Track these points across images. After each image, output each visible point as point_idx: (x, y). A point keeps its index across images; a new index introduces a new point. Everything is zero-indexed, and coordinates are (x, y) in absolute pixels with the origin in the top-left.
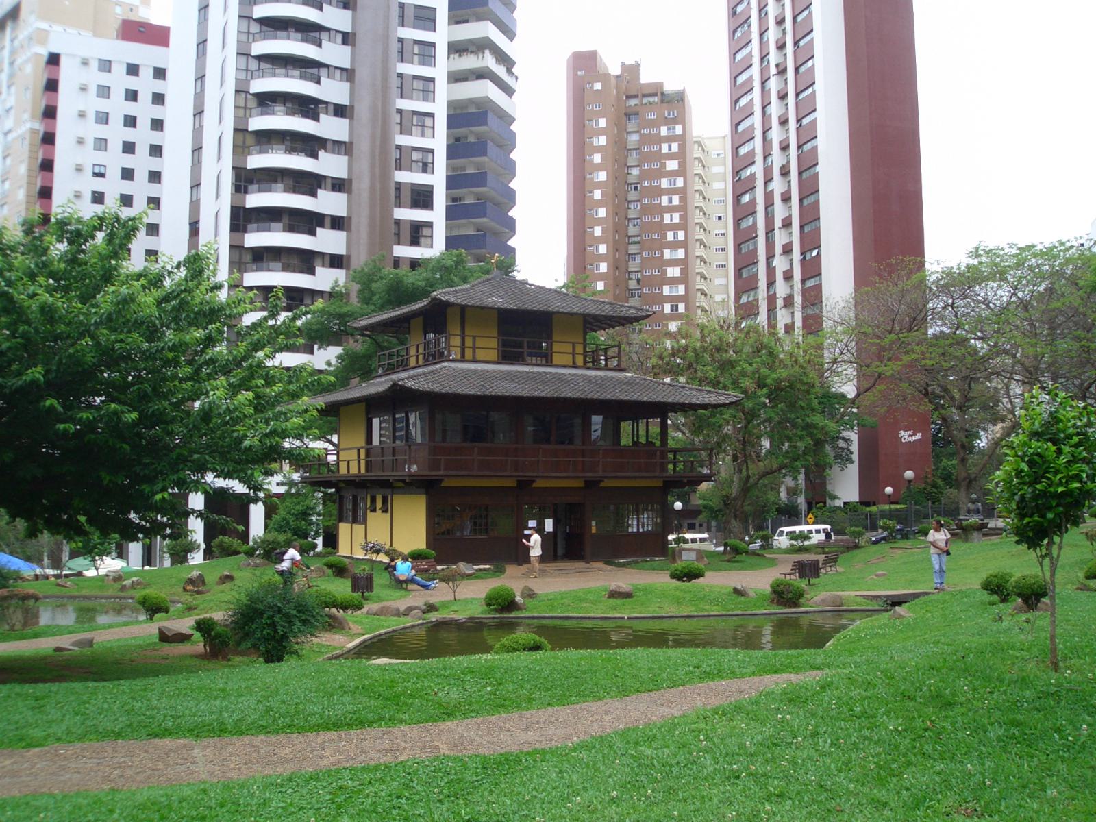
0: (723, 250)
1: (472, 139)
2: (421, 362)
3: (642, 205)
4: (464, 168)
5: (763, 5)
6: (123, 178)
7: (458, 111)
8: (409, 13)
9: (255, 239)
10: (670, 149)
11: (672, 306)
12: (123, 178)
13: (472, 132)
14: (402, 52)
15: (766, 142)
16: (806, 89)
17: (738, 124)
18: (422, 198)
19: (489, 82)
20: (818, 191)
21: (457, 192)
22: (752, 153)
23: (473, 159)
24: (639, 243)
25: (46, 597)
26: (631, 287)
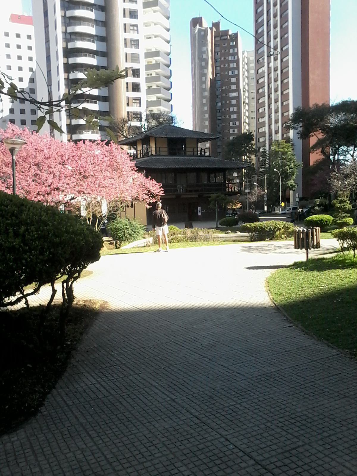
1: (154, 62)
4: (151, 74)
6: (19, 70)
7: (148, 51)
8: (129, 58)
9: (71, 61)
10: (233, 65)
11: (233, 123)
12: (19, 70)
14: (125, 29)
15: (269, 79)
16: (285, 68)
17: (258, 50)
22: (263, 72)
26: (217, 94)
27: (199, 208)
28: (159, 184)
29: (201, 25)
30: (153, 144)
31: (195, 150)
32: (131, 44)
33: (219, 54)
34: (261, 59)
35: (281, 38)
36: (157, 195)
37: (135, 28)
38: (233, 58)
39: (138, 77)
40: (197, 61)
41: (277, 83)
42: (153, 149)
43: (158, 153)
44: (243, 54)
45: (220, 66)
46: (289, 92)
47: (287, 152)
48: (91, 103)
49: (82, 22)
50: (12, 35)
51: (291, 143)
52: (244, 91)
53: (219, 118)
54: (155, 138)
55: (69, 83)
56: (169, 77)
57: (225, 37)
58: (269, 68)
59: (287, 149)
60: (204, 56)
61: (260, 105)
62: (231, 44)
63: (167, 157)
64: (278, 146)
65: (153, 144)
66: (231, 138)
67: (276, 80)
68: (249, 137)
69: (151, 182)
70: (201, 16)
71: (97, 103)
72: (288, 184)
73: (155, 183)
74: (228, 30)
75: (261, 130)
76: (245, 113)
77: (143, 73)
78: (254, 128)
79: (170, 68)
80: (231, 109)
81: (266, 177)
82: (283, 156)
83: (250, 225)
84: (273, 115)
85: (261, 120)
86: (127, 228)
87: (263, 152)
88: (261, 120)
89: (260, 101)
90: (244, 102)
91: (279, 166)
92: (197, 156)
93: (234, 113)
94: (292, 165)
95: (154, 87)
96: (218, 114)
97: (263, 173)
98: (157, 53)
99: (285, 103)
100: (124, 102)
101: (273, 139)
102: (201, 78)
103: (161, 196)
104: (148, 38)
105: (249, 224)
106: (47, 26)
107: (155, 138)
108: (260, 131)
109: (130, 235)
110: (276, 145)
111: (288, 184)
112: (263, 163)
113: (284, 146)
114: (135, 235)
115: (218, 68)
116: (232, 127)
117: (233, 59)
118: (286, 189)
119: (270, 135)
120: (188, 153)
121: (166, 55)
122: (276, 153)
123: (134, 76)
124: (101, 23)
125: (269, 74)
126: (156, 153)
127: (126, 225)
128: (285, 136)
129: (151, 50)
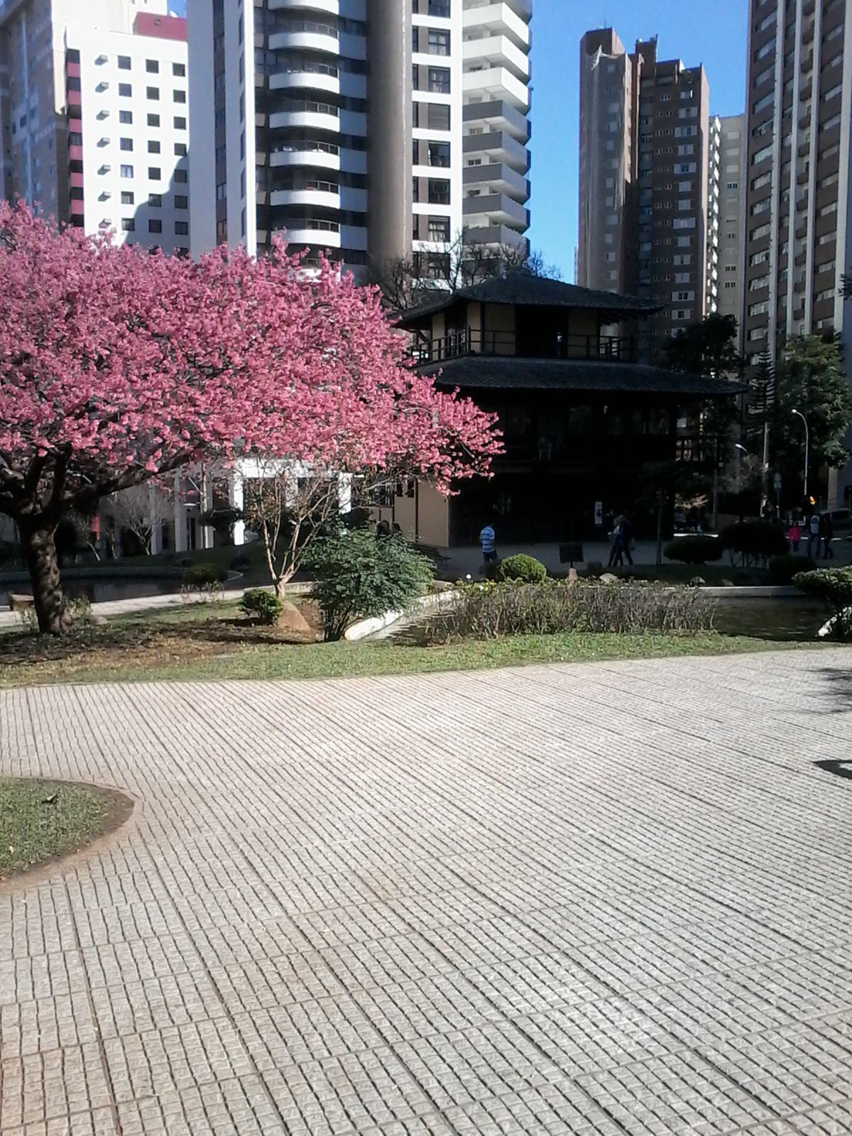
0: (735, 186)
1: (486, 130)
2: (442, 357)
3: (654, 211)
4: (479, 162)
5: (784, 160)
13: (488, 123)
17: (757, 103)
18: (439, 154)
19: (504, 70)
20: (838, 172)
21: (473, 186)
22: (769, 160)
23: (487, 151)
24: (650, 285)
25: (65, 44)
26: (641, 223)
27: (598, 505)
28: (487, 416)
29: (608, 49)
30: (474, 323)
31: (593, 342)
32: (431, 81)
33: (651, 121)
34: (763, 127)
35: (821, 70)
36: (478, 454)
37: (442, 40)
38: (686, 131)
39: (443, 166)
40: (595, 138)
41: (805, 188)
42: (476, 336)
43: (489, 347)
44: (711, 125)
45: (652, 152)
46: (836, 211)
47: (824, 367)
48: (322, 229)
49: (306, 23)
50: (139, 65)
51: (837, 343)
52: (709, 217)
53: (645, 281)
54: (483, 306)
55: (270, 178)
56: (522, 200)
57: (670, 79)
58: (784, 149)
59: (828, 359)
60: (613, 127)
61: (755, 246)
62: (683, 95)
63: (514, 360)
64: (801, 349)
65: (474, 323)
66: (674, 332)
67: (802, 180)
68: (722, 326)
69: (460, 408)
70: (608, 27)
71: (337, 231)
72: (825, 449)
73: (476, 410)
74: (677, 62)
75: (757, 310)
76: (709, 272)
77: (457, 156)
78: (735, 309)
79: (528, 146)
80: (677, 260)
81: (766, 431)
82: (815, 378)
83: (838, 575)
84: (790, 270)
85: (758, 284)
86: (367, 567)
87: (761, 365)
88: (758, 284)
89: (757, 236)
90: (708, 245)
91: (803, 401)
92: (598, 358)
93: (682, 269)
94: (839, 401)
95: (485, 192)
96: (643, 272)
97: (760, 419)
98: (495, 107)
99: (823, 241)
100: (406, 228)
101: (789, 331)
102: (602, 182)
103: (495, 456)
104: (474, 69)
105: (833, 570)
106: (219, 36)
107: (483, 306)
108: (754, 311)
109: (378, 590)
110: (797, 346)
111: (825, 449)
112: (760, 395)
113: (819, 349)
114: (397, 592)
115: (647, 157)
116: (676, 306)
117: (685, 134)
118: (819, 460)
119: (781, 322)
120: (571, 352)
121: (518, 113)
122: (795, 368)
123: (434, 164)
124: (355, 26)
125: (784, 162)
126: (483, 347)
127: (367, 554)
128: (820, 325)
129: (481, 98)
